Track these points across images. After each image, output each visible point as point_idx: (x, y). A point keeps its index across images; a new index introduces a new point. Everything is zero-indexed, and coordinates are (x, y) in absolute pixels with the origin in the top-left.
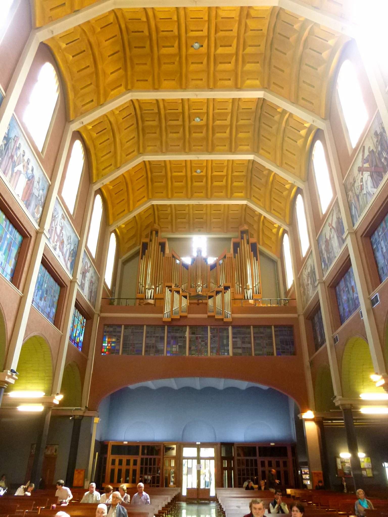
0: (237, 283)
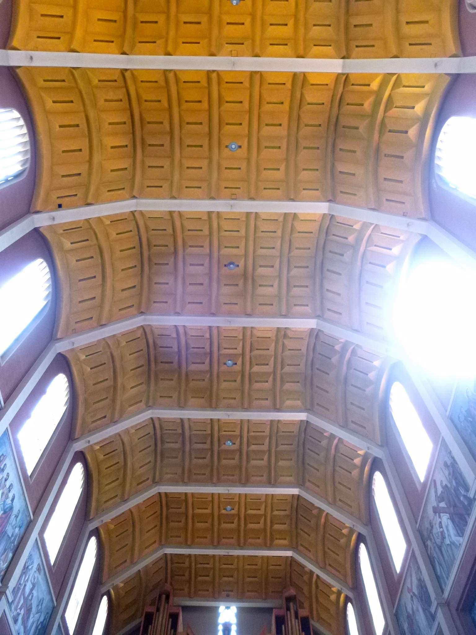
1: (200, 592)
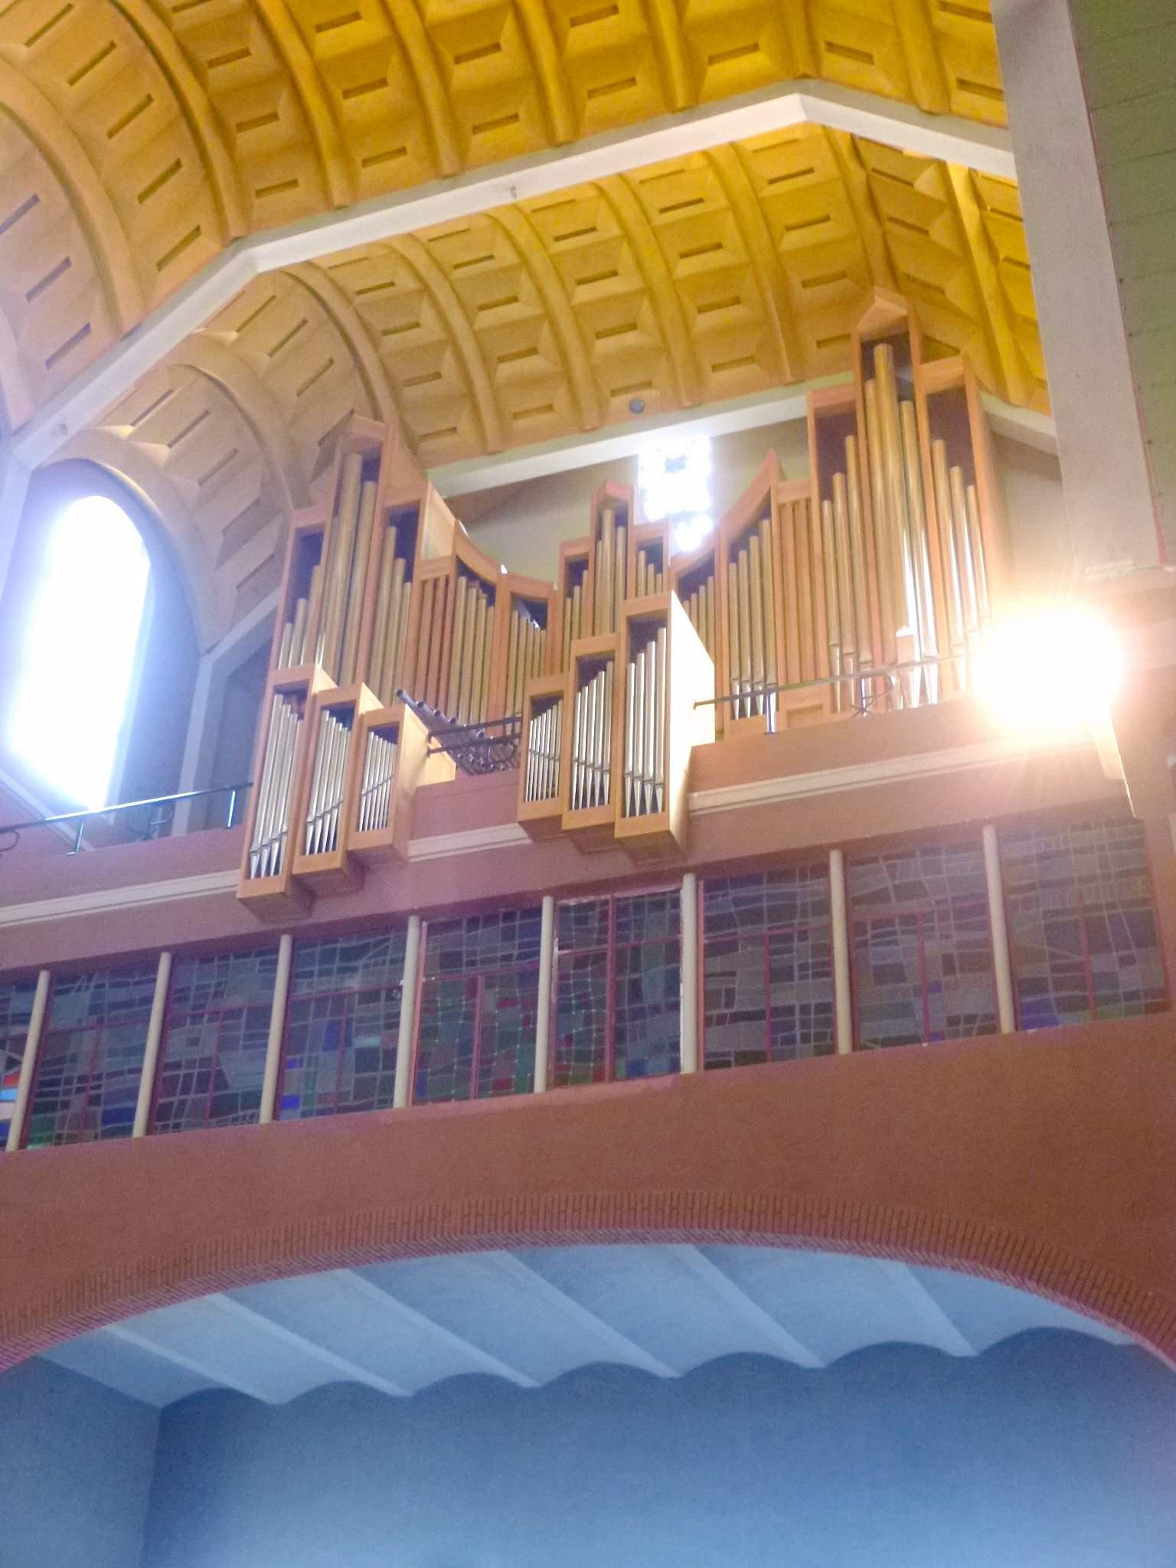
0: (841, 645)
1: (522, 423)
